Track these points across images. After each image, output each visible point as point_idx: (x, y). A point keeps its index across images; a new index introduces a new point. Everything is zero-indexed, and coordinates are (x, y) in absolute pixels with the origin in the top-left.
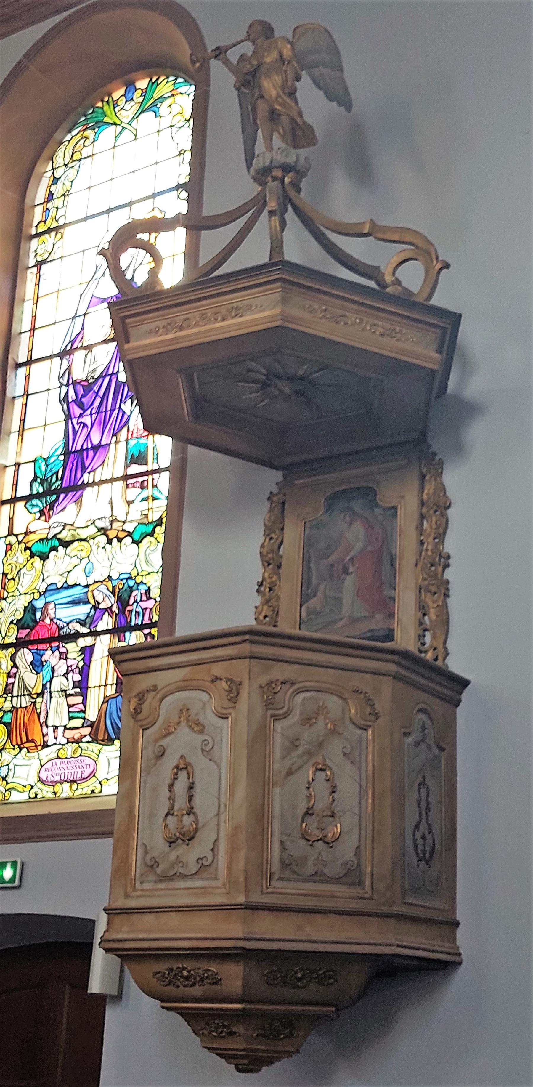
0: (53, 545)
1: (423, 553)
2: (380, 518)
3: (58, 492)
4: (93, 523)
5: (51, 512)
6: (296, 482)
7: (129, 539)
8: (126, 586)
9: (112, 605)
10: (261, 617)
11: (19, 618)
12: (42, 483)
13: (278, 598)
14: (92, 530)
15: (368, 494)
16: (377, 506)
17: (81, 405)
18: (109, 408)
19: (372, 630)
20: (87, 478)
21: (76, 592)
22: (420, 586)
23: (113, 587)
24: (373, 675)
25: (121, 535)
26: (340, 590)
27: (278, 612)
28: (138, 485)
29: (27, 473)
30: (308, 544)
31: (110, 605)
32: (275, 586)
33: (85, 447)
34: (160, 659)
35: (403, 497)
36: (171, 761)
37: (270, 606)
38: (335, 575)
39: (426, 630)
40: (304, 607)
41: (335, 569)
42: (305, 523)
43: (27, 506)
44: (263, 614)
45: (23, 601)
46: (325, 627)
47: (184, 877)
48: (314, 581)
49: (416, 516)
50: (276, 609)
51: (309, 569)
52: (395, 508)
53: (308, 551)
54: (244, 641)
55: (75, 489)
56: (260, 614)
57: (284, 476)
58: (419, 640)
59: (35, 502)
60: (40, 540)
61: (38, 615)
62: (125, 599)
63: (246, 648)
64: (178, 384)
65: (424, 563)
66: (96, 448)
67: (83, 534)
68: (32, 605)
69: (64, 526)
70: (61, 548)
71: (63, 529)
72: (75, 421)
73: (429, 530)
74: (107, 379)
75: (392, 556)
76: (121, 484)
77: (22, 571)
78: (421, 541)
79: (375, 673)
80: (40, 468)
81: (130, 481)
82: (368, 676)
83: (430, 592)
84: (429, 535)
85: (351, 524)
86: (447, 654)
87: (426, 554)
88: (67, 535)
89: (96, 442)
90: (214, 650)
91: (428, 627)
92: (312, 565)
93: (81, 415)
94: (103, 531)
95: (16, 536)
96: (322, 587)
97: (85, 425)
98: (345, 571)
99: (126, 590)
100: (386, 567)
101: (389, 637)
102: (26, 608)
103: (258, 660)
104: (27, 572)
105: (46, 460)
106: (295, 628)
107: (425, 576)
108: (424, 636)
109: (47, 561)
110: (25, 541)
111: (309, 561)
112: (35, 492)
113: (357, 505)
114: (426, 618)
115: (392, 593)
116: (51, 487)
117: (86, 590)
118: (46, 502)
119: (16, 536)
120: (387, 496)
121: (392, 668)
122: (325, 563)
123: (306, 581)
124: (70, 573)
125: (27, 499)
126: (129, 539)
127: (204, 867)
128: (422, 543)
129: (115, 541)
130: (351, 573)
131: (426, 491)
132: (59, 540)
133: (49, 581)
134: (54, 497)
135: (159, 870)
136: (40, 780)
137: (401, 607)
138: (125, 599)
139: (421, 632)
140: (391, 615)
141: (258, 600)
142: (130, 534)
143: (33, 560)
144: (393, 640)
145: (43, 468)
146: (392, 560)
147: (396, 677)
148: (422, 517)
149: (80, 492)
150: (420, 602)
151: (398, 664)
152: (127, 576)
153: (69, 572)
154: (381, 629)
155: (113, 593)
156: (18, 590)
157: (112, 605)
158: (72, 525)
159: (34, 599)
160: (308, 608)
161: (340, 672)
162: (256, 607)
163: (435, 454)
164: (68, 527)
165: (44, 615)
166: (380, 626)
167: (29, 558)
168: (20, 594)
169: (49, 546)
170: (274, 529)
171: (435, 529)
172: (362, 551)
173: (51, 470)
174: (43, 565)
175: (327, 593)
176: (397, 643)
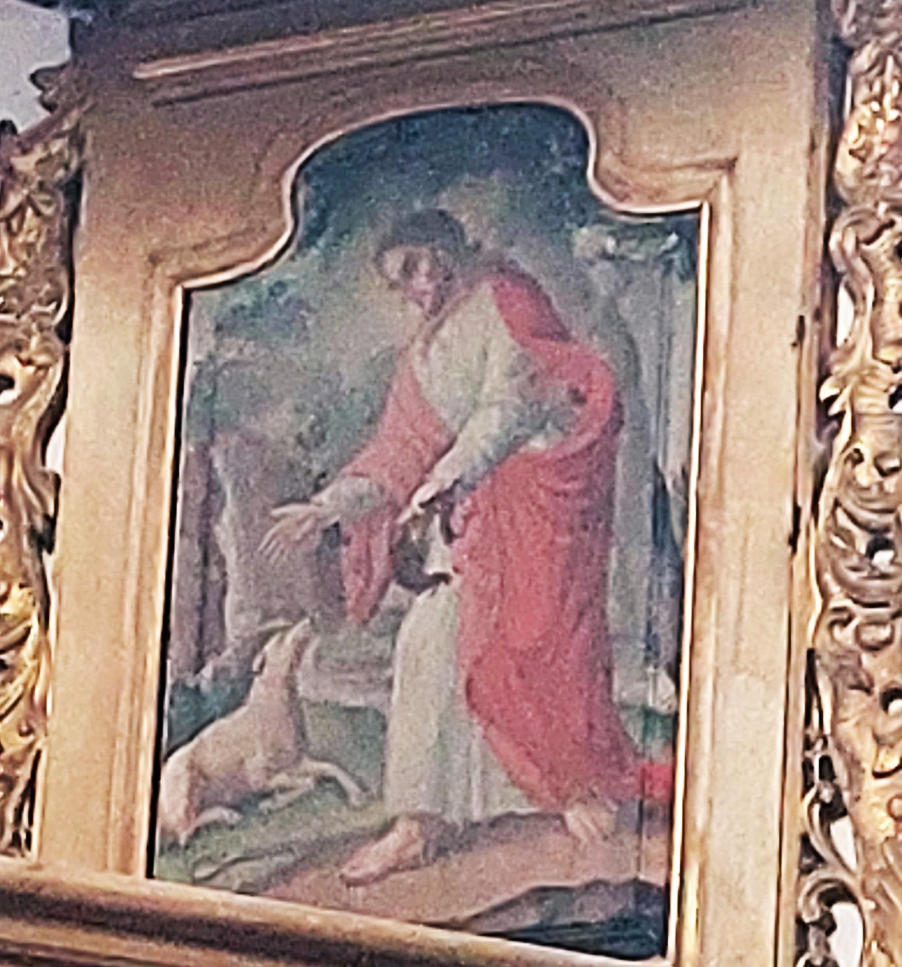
1: (832, 478)
2: (601, 277)
15: (543, 152)
16: (587, 209)
19: (543, 892)
30: (201, 411)
38: (352, 585)
39: (839, 893)
40: (174, 766)
41: (347, 554)
46: (285, 874)
48: (237, 623)
49: (798, 270)
50: (24, 773)
52: (684, 225)
53: (203, 455)
57: (76, 36)
73: (865, 344)
75: (660, 491)
78: (824, 405)
84: (865, 377)
85: (438, 308)
87: (849, 482)
91: (853, 884)
92: (225, 532)
96: (276, 653)
98: (408, 569)
106: (125, 869)
107: (839, 600)
108: (828, 925)
111: (208, 513)
113: (477, 207)
114: (841, 829)
115: (660, 694)
120: (649, 154)
123: (193, 617)
130: (443, 578)
131: (851, 137)
136: (567, 434)
139: (812, 913)
148: (831, 276)
150: (808, 745)
160: (196, 770)
172: (510, 447)
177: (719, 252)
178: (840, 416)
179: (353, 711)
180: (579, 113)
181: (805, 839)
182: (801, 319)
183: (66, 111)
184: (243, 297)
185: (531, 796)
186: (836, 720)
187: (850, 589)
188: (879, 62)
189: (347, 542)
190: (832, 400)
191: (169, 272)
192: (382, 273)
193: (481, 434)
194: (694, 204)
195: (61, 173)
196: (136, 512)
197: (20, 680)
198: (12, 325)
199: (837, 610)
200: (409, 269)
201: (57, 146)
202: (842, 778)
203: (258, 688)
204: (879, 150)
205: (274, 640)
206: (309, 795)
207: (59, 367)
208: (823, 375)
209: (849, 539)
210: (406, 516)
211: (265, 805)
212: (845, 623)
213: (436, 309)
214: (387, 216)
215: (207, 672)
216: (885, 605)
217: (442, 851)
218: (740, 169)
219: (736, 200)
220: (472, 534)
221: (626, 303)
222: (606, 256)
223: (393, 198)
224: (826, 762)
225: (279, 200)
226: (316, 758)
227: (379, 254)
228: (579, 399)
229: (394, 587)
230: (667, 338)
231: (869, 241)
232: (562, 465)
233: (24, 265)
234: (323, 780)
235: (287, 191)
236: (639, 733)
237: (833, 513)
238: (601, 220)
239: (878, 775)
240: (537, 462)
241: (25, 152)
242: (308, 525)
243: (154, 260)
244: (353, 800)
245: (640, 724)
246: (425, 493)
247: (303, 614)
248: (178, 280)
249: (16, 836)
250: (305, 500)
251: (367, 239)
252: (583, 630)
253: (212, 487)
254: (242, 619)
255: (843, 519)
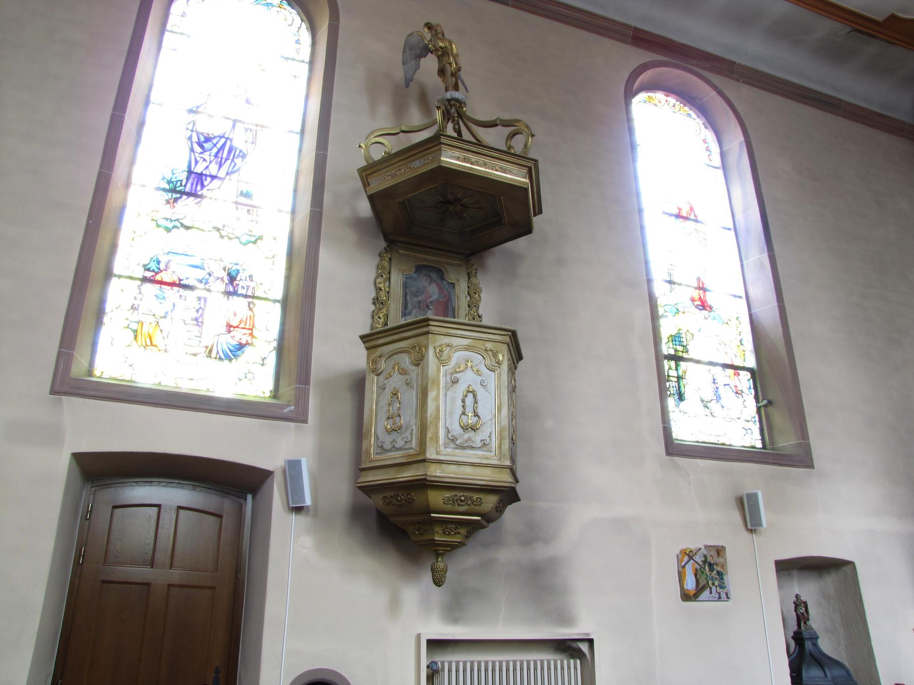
3: (183, 193)
17: (202, 147)
18: (224, 156)
36: (461, 388)
47: (472, 448)
48: (410, 307)
66: (213, 177)
74: (223, 140)
93: (201, 153)
97: (205, 160)
120: (451, 276)
127: (485, 445)
135: (458, 442)
172: (437, 300)
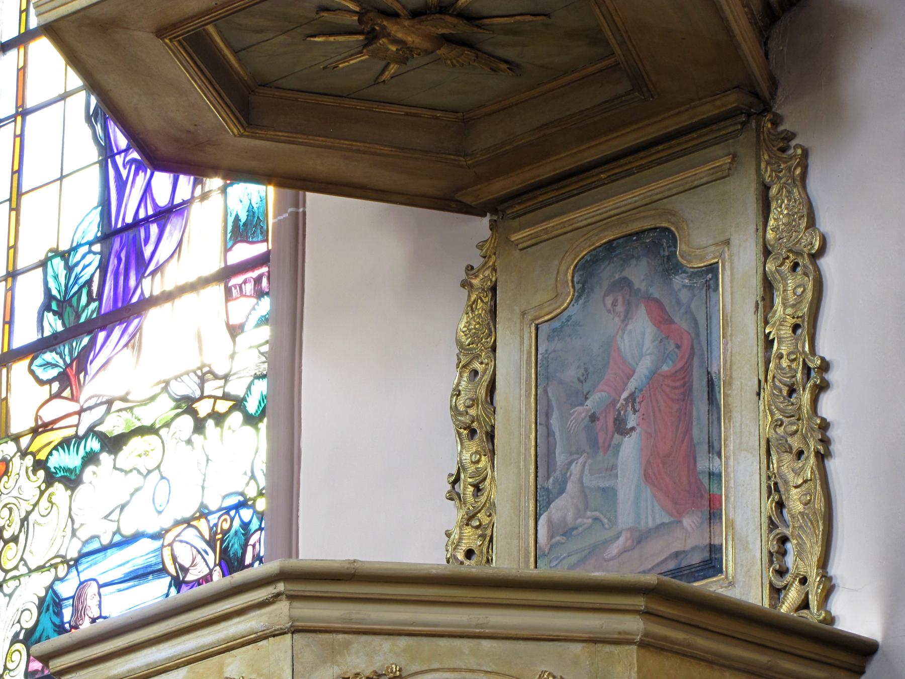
0: (88, 450)
2: (684, 295)
4: (165, 389)
5: (82, 376)
6: (514, 237)
7: (237, 416)
8: (237, 523)
9: (211, 571)
10: (460, 556)
11: (29, 625)
12: (59, 314)
13: (491, 508)
14: (163, 408)
19: (677, 554)
20: (149, 287)
21: (140, 554)
22: (768, 441)
23: (211, 529)
24: (591, 647)
25: (223, 406)
26: (612, 469)
27: (491, 540)
28: (249, 288)
29: (30, 292)
30: (543, 373)
31: (207, 571)
32: (484, 479)
33: (142, 215)
34: (132, 656)
35: (727, 243)
37: (477, 527)
41: (598, 424)
42: (537, 329)
43: (33, 367)
44: (464, 547)
45: (33, 588)
48: (560, 458)
49: (755, 284)
50: (489, 532)
51: (549, 434)
52: (712, 269)
54: (277, 596)
55: (124, 312)
56: (457, 546)
57: (493, 226)
58: (771, 562)
59: (49, 356)
60: (61, 444)
61: (67, 613)
62: (235, 554)
63: (281, 612)
64: (315, 42)
65: (775, 387)
66: (163, 215)
67: (147, 416)
68: (55, 592)
69: (110, 403)
70: (105, 457)
71: (108, 411)
72: (119, 159)
76: (217, 290)
77: (32, 518)
78: (767, 336)
79: (594, 640)
80: (56, 277)
81: (237, 280)
82: (577, 648)
83: (789, 450)
85: (627, 318)
86: (828, 590)
87: (779, 367)
88: (113, 426)
89: (163, 201)
90: (223, 625)
92: (554, 421)
94: (187, 405)
95: (16, 439)
96: (575, 469)
98: (621, 427)
99: (236, 533)
100: (700, 406)
101: (712, 563)
102: (42, 601)
103: (313, 635)
104: (41, 520)
105: (64, 256)
107: (778, 416)
109: (81, 489)
110: (33, 448)
111: (548, 416)
112: (47, 333)
113: (639, 272)
116: (78, 316)
117: (157, 544)
118: (71, 353)
119: (16, 439)
120: (696, 244)
121: (634, 625)
122: (581, 413)
123: (544, 460)
124: (126, 509)
125: (34, 350)
126: (237, 416)
128: (769, 343)
129: (210, 423)
130: (633, 429)
131: (772, 222)
132: (102, 437)
133: (83, 534)
134: (86, 340)
137: (732, 492)
138: (235, 554)
140: (713, 513)
141: (453, 514)
142: (239, 404)
143: (50, 490)
144: (721, 571)
145: (62, 273)
146: (711, 386)
147: (647, 644)
149: (136, 321)
150: (769, 478)
151: (647, 613)
152: (234, 500)
153: (123, 507)
154: (694, 549)
155: (211, 543)
156: (26, 564)
157: (211, 571)
158: (124, 399)
159: (57, 579)
160: (550, 523)
161: (508, 644)
162: (448, 535)
163: (789, 136)
164: (117, 405)
165: (78, 612)
166: (692, 542)
167: (43, 487)
168: (31, 571)
169: (82, 452)
170: (478, 350)
171: (793, 306)
172: (653, 373)
173: (76, 282)
174: (71, 497)
175: (586, 480)
176: (727, 577)
177: (724, 278)
178: (774, 339)
179: (604, 490)
180: (673, 229)
181: (770, 518)
182: (757, 302)
183: (490, 257)
184: (556, 324)
185: (671, 515)
186: (779, 467)
187: (781, 411)
188: (779, 191)
189: (598, 419)
190: (770, 333)
191: (530, 317)
192: (605, 305)
193: (644, 367)
194: (716, 260)
195: (489, 283)
196: (523, 416)
197: (486, 494)
198: (475, 349)
199: (777, 421)
200: (614, 304)
201: (487, 273)
202: (782, 490)
203: (570, 486)
204: (782, 227)
205: (574, 464)
206: (589, 527)
207: (493, 363)
208: (766, 322)
209: (781, 391)
210: (619, 405)
211: (575, 532)
212: (781, 425)
213: (624, 320)
214: (606, 284)
215: (551, 481)
216: (793, 416)
217: (639, 542)
218: (732, 242)
219: (731, 256)
220: (642, 411)
221: (693, 306)
222: (684, 286)
223: (607, 273)
224: (776, 484)
225: (567, 282)
226: (591, 511)
227: (604, 300)
228: (678, 347)
229: (616, 435)
230: (708, 318)
231: (780, 266)
232: (673, 375)
233: (478, 323)
234: (596, 519)
235: (570, 278)
236: (707, 481)
237: (773, 381)
238: (684, 272)
239: (796, 487)
240: (665, 376)
241: (476, 277)
242: (583, 415)
243: (523, 314)
244: (607, 526)
245: (707, 478)
246: (625, 395)
247: (584, 451)
248: (533, 320)
249: (488, 559)
250: (582, 404)
251: (598, 293)
252: (685, 444)
253: (549, 405)
254: (562, 457)
255: (777, 383)
